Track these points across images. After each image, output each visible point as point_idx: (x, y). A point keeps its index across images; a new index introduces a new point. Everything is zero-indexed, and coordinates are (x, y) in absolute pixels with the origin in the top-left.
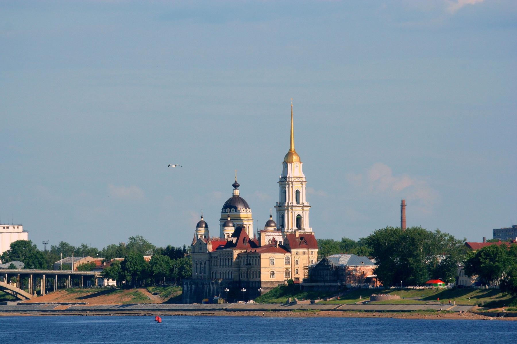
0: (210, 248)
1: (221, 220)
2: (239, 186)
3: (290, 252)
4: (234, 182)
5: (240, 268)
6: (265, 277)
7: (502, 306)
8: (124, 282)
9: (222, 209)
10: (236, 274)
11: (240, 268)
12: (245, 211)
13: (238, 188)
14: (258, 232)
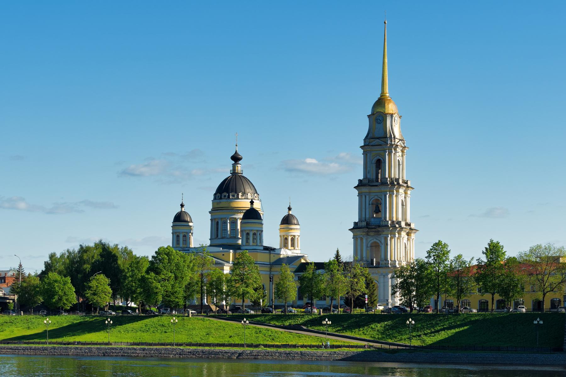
0: (124, 248)
2: (240, 159)
12: (257, 199)
13: (240, 162)
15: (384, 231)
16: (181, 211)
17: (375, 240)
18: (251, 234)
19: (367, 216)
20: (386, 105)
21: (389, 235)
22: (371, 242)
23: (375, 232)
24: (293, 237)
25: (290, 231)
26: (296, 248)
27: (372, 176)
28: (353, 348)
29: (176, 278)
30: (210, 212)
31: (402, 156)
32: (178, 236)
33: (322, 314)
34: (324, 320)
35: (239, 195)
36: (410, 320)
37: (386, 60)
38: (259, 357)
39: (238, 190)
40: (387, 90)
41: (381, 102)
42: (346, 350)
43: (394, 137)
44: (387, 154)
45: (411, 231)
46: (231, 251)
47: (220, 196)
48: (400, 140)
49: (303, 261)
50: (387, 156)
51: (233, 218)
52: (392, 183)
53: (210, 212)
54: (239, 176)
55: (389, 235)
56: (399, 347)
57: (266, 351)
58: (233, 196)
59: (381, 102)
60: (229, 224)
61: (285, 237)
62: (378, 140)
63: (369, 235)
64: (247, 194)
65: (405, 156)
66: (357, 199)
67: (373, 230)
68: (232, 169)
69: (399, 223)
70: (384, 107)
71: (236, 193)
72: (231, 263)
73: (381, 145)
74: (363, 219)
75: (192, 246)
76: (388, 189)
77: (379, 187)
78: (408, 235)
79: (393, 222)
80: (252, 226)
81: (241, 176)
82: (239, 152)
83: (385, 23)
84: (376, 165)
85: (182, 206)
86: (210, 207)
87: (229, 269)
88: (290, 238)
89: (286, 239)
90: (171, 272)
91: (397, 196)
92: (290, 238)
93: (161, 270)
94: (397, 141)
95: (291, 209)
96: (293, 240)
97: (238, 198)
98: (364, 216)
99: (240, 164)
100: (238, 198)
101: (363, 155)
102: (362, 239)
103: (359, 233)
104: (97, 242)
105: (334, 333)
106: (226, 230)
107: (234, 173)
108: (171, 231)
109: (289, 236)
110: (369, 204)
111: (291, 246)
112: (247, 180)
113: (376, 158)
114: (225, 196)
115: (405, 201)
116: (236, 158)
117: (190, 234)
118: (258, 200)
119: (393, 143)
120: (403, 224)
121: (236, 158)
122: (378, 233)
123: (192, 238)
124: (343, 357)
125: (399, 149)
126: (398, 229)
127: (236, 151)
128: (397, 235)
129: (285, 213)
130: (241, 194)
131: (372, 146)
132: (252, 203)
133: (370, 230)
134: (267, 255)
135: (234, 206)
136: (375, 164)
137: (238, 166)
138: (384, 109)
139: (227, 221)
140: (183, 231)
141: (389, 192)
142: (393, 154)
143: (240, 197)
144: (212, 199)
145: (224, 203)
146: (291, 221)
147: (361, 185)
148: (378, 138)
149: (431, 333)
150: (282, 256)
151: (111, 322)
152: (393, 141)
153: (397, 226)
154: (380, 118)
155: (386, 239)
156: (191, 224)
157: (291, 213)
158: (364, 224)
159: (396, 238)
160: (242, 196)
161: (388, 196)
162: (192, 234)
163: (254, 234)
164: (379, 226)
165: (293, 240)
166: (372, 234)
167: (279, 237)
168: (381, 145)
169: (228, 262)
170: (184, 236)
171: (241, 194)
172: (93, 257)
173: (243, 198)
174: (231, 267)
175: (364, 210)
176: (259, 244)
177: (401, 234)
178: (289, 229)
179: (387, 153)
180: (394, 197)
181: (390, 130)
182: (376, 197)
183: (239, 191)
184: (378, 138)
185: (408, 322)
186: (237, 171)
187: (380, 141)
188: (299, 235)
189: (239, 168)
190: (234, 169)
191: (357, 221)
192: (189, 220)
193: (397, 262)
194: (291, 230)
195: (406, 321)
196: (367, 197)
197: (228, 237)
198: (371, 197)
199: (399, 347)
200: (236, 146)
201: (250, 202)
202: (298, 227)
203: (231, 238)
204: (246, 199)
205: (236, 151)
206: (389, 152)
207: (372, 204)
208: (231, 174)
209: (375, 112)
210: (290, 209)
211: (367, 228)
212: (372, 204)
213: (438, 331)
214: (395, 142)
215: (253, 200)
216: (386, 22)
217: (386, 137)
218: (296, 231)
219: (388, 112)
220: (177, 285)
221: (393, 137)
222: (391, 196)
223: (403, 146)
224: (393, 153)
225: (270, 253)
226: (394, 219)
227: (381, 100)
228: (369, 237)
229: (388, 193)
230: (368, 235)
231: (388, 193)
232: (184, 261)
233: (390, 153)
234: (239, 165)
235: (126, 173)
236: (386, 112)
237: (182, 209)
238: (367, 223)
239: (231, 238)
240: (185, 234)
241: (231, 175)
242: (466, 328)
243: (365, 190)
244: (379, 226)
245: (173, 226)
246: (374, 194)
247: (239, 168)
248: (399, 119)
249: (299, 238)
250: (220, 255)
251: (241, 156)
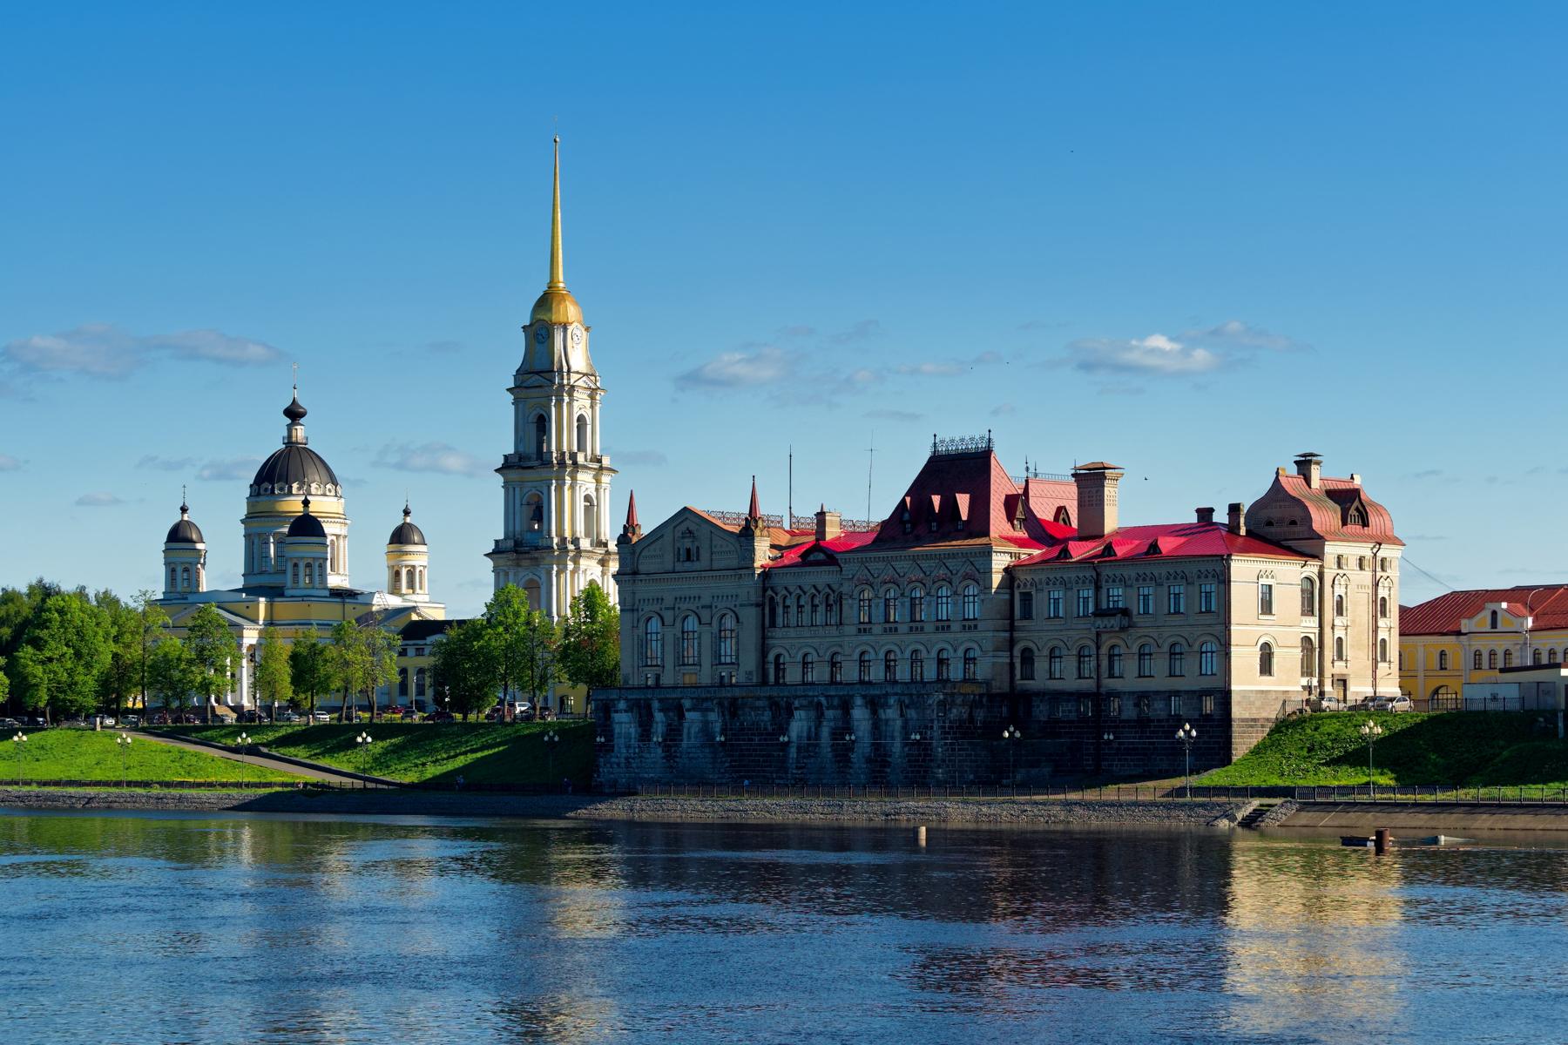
0: (763, 554)
1: (247, 518)
2: (303, 415)
3: (1318, 556)
4: (288, 403)
5: (1016, 634)
6: (1244, 679)
7: (1275, 797)
8: (447, 700)
9: (251, 486)
10: (1000, 660)
11: (1016, 634)
12: (333, 493)
13: (302, 421)
14: (1298, 459)
15: (544, 558)
16: (182, 520)
17: (531, 576)
18: (302, 565)
19: (518, 528)
22: (524, 580)
23: (531, 559)
25: (405, 558)
26: (418, 591)
27: (532, 449)
29: (78, 655)
30: (243, 521)
31: (592, 407)
32: (173, 570)
33: (312, 724)
34: (17, 734)
36: (364, 735)
38: (115, 805)
39: (291, 473)
41: (546, 301)
42: (234, 792)
43: (569, 371)
45: (607, 557)
46: (262, 600)
48: (584, 375)
49: (415, 617)
50: (553, 409)
51: (279, 533)
52: (562, 463)
53: (243, 521)
56: (380, 786)
58: (281, 489)
59: (546, 301)
60: (272, 545)
61: (396, 568)
62: (537, 377)
63: (520, 566)
67: (527, 556)
68: (286, 434)
69: (575, 541)
70: (550, 310)
72: (261, 622)
73: (540, 386)
74: (511, 535)
75: (204, 587)
76: (554, 475)
78: (603, 566)
79: (563, 540)
80: (303, 549)
83: (555, 141)
84: (537, 427)
86: (243, 511)
87: (257, 636)
89: (398, 574)
90: (67, 645)
91: (572, 487)
92: (404, 572)
93: (46, 642)
94: (574, 377)
96: (411, 574)
97: (290, 493)
98: (511, 529)
100: (290, 493)
102: (507, 574)
103: (502, 562)
104: (34, 582)
105: (302, 760)
106: (268, 556)
107: (290, 443)
111: (408, 588)
112: (314, 456)
113: (535, 412)
114: (266, 490)
115: (597, 498)
116: (294, 414)
117: (199, 566)
118: (336, 496)
119: (565, 382)
120: (585, 544)
121: (294, 414)
122: (536, 562)
123: (203, 574)
124: (235, 803)
126: (571, 554)
128: (570, 566)
131: (526, 388)
132: (306, 503)
133: (521, 556)
134: (339, 607)
139: (269, 539)
140: (182, 560)
141: (556, 480)
142: (565, 404)
143: (294, 491)
145: (264, 504)
147: (508, 466)
148: (538, 373)
149: (443, 759)
150: (374, 609)
151: (1194, 733)
152: (565, 377)
153: (571, 547)
154: (543, 332)
156: (199, 546)
157: (408, 520)
158: (511, 543)
160: (299, 489)
161: (553, 488)
162: (203, 565)
163: (308, 565)
164: (537, 548)
165: (411, 574)
166: (525, 563)
168: (540, 386)
169: (255, 621)
170: (186, 570)
172: (18, 613)
174: (261, 632)
175: (511, 516)
176: (317, 585)
181: (561, 356)
182: (534, 491)
184: (538, 373)
185: (1181, 733)
186: (294, 439)
188: (425, 564)
189: (300, 432)
190: (290, 436)
191: (501, 537)
192: (194, 537)
195: (1003, 732)
196: (517, 490)
197: (272, 571)
198: (525, 490)
199: (380, 786)
203: (277, 573)
206: (557, 400)
207: (528, 504)
211: (516, 552)
212: (528, 504)
213: (456, 756)
214: (569, 379)
215: (309, 498)
217: (553, 371)
218: (418, 557)
220: (80, 669)
221: (565, 369)
222: (560, 489)
223: (593, 387)
225: (344, 603)
228: (520, 569)
230: (518, 565)
232: (98, 624)
233: (560, 402)
234: (298, 427)
235: (693, 379)
238: (516, 542)
239: (277, 573)
240: (309, 561)
242: (501, 748)
243: (514, 475)
244: (537, 548)
246: (530, 484)
247: (300, 432)
248: (585, 333)
249: (426, 572)
250: (241, 608)
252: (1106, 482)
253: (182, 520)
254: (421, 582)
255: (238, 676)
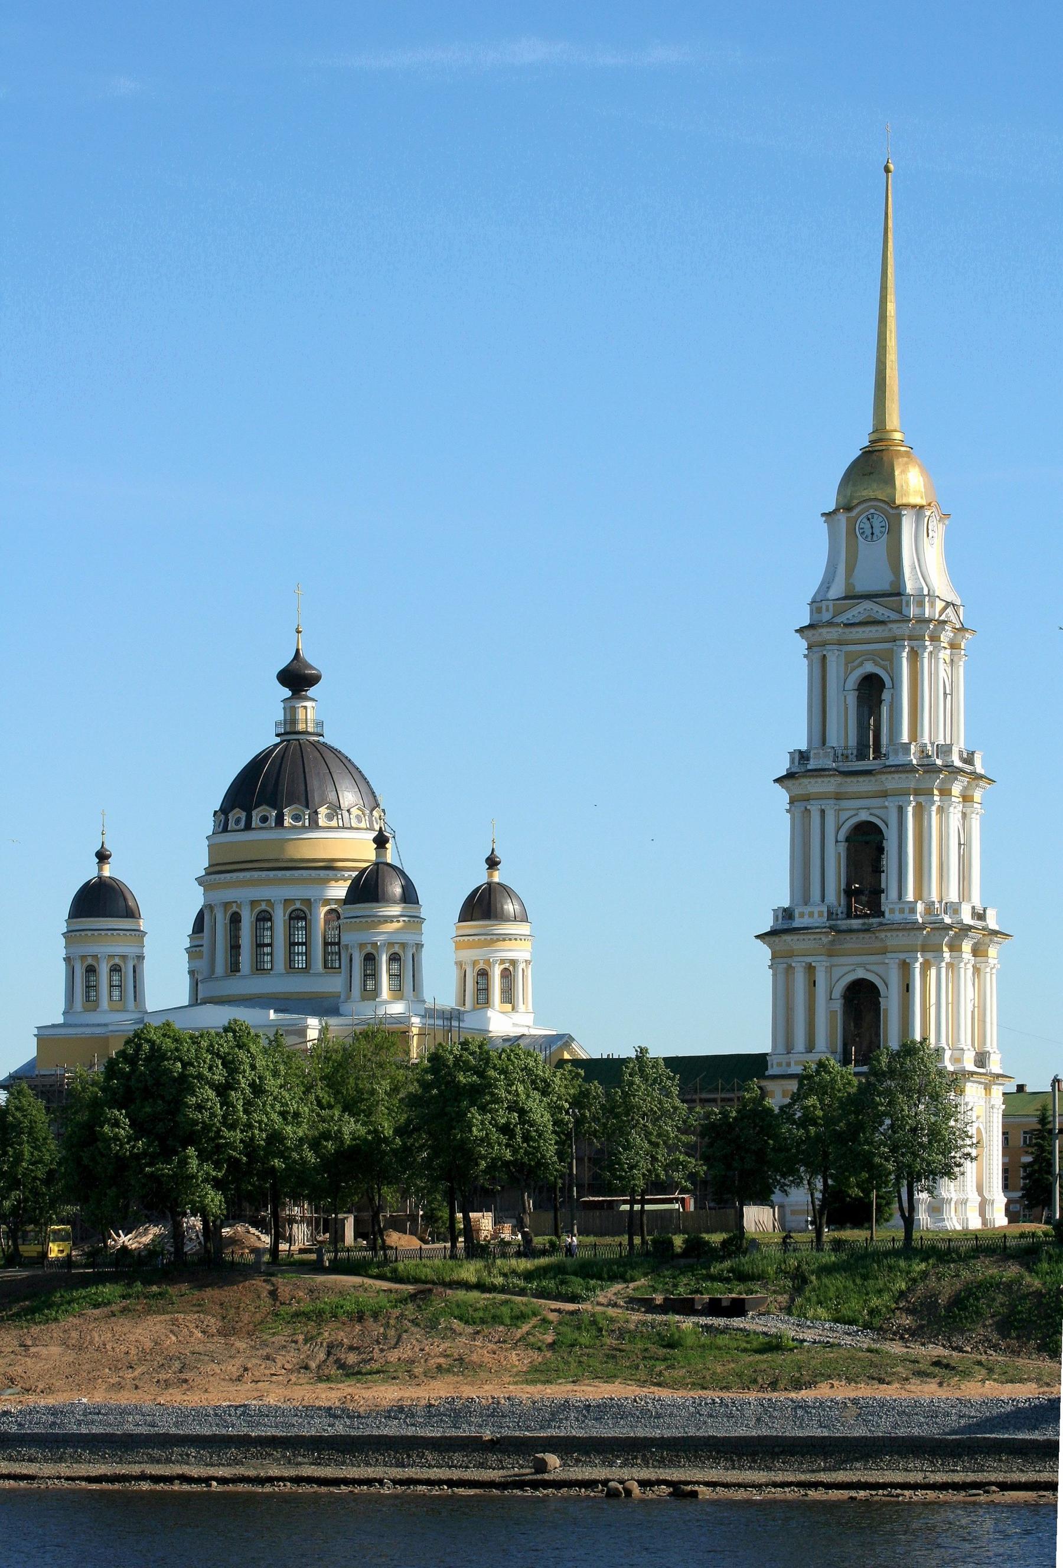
2: (313, 680)
4: (284, 661)
9: (216, 812)
13: (312, 692)
20: (897, 473)
21: (919, 955)
24: (511, 969)
25: (500, 945)
28: (548, 1382)
30: (200, 881)
35: (316, 813)
37: (891, 307)
40: (893, 420)
44: (905, 654)
45: (987, 939)
47: (244, 819)
53: (200, 881)
54: (312, 744)
55: (919, 955)
57: (856, 1383)
58: (296, 818)
62: (867, 605)
64: (348, 811)
65: (961, 663)
66: (784, 823)
68: (280, 716)
71: (307, 807)
73: (882, 623)
77: (879, 777)
81: (318, 742)
82: (304, 654)
83: (887, 170)
85: (102, 857)
86: (201, 862)
88: (496, 972)
91: (941, 810)
92: (496, 972)
95: (498, 863)
96: (507, 975)
97: (314, 825)
99: (313, 700)
100: (314, 825)
101: (805, 661)
107: (289, 730)
108: (63, 953)
109: (495, 962)
110: (837, 841)
125: (946, 636)
127: (298, 651)
129: (479, 877)
130: (327, 811)
135: (299, 857)
136: (856, 693)
137: (305, 708)
138: (889, 491)
142: (926, 655)
144: (209, 831)
146: (499, 906)
155: (906, 968)
159: (943, 964)
160: (330, 817)
161: (910, 809)
165: (507, 975)
167: (455, 967)
168: (882, 623)
171: (327, 811)
173: (334, 823)
177: (960, 950)
178: (495, 937)
179: (907, 650)
180: (934, 814)
183: (317, 799)
187: (876, 608)
188: (529, 958)
189: (309, 713)
190: (290, 720)
193: (948, 1054)
194: (504, 940)
198: (844, 815)
200: (298, 632)
201: (375, 840)
202: (523, 929)
204: (343, 828)
205: (298, 651)
208: (277, 735)
209: (855, 502)
210: (492, 863)
216: (891, 167)
219: (905, 501)
224: (928, 650)
226: (935, 897)
227: (874, 457)
229: (912, 799)
231: (912, 799)
233: (915, 656)
234: (308, 704)
236: (898, 502)
237: (100, 869)
241: (278, 739)
245: (68, 932)
247: (309, 713)
251: (315, 669)
252: (885, 690)
253: (100, 878)
254: (293, 1025)
255: (981, 1023)
